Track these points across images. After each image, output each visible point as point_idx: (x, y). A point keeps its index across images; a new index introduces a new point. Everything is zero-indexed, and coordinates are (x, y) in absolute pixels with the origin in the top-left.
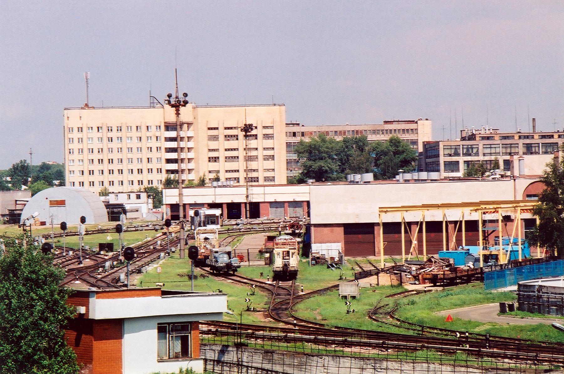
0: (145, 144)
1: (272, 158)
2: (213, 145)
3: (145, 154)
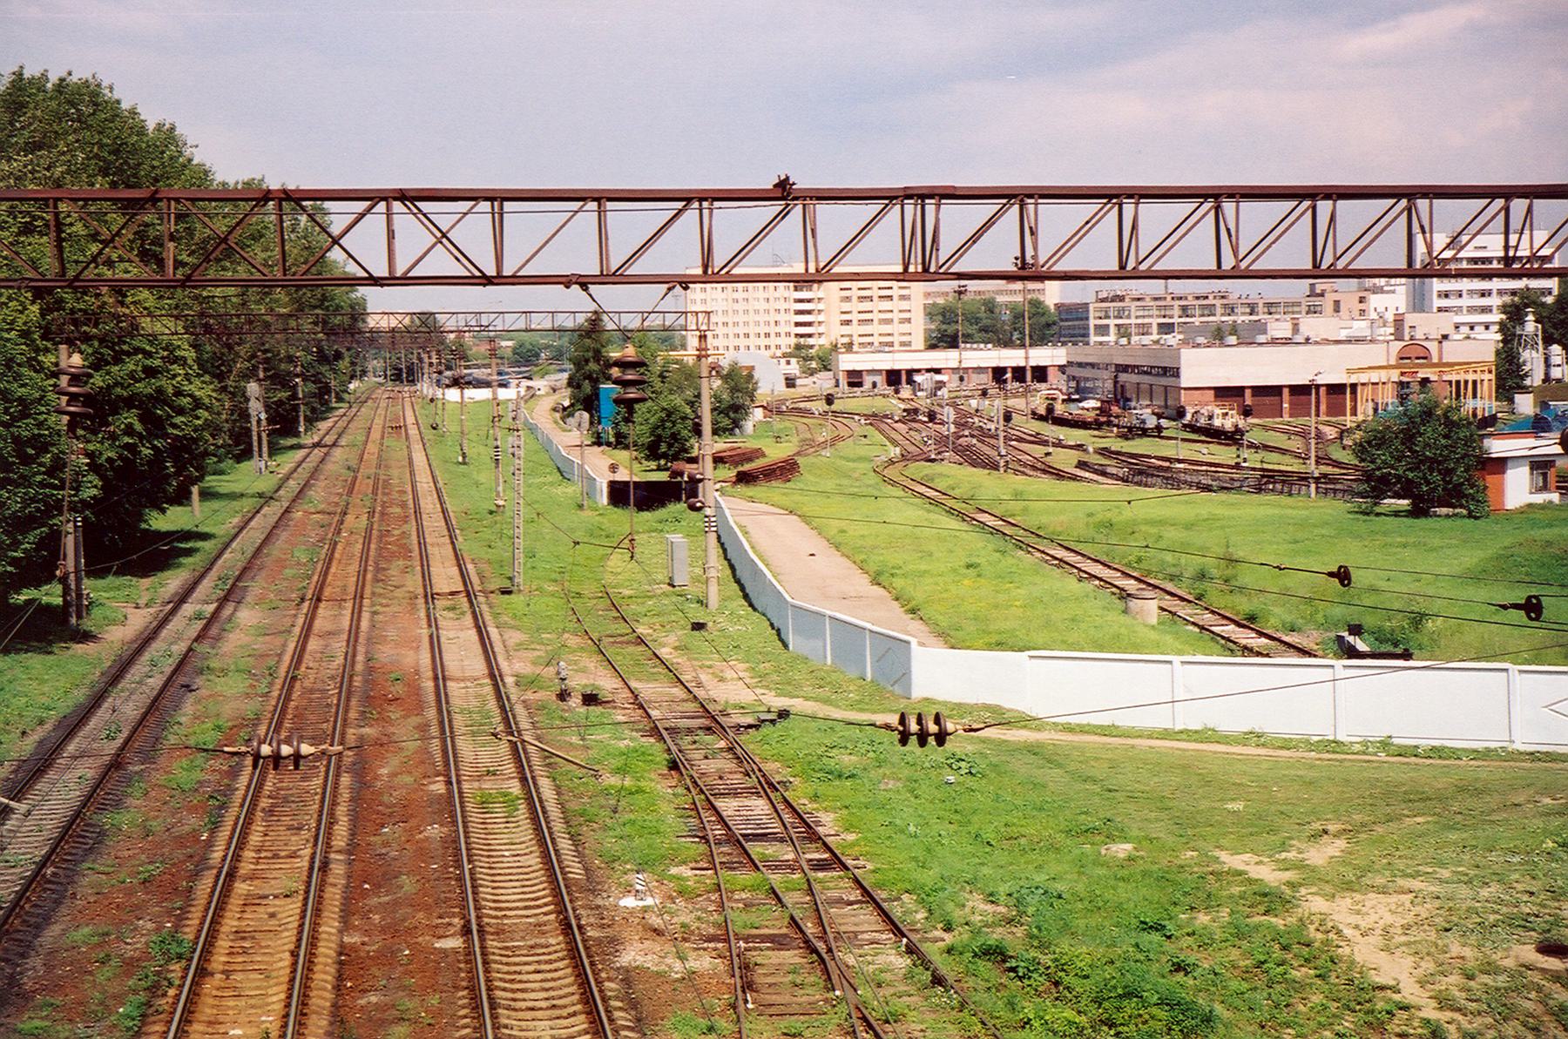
0: (773, 305)
1: (909, 321)
2: (846, 306)
3: (773, 317)
